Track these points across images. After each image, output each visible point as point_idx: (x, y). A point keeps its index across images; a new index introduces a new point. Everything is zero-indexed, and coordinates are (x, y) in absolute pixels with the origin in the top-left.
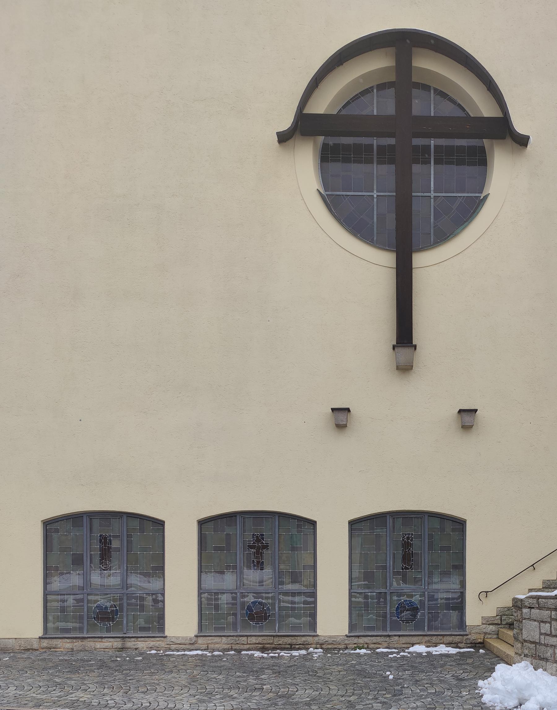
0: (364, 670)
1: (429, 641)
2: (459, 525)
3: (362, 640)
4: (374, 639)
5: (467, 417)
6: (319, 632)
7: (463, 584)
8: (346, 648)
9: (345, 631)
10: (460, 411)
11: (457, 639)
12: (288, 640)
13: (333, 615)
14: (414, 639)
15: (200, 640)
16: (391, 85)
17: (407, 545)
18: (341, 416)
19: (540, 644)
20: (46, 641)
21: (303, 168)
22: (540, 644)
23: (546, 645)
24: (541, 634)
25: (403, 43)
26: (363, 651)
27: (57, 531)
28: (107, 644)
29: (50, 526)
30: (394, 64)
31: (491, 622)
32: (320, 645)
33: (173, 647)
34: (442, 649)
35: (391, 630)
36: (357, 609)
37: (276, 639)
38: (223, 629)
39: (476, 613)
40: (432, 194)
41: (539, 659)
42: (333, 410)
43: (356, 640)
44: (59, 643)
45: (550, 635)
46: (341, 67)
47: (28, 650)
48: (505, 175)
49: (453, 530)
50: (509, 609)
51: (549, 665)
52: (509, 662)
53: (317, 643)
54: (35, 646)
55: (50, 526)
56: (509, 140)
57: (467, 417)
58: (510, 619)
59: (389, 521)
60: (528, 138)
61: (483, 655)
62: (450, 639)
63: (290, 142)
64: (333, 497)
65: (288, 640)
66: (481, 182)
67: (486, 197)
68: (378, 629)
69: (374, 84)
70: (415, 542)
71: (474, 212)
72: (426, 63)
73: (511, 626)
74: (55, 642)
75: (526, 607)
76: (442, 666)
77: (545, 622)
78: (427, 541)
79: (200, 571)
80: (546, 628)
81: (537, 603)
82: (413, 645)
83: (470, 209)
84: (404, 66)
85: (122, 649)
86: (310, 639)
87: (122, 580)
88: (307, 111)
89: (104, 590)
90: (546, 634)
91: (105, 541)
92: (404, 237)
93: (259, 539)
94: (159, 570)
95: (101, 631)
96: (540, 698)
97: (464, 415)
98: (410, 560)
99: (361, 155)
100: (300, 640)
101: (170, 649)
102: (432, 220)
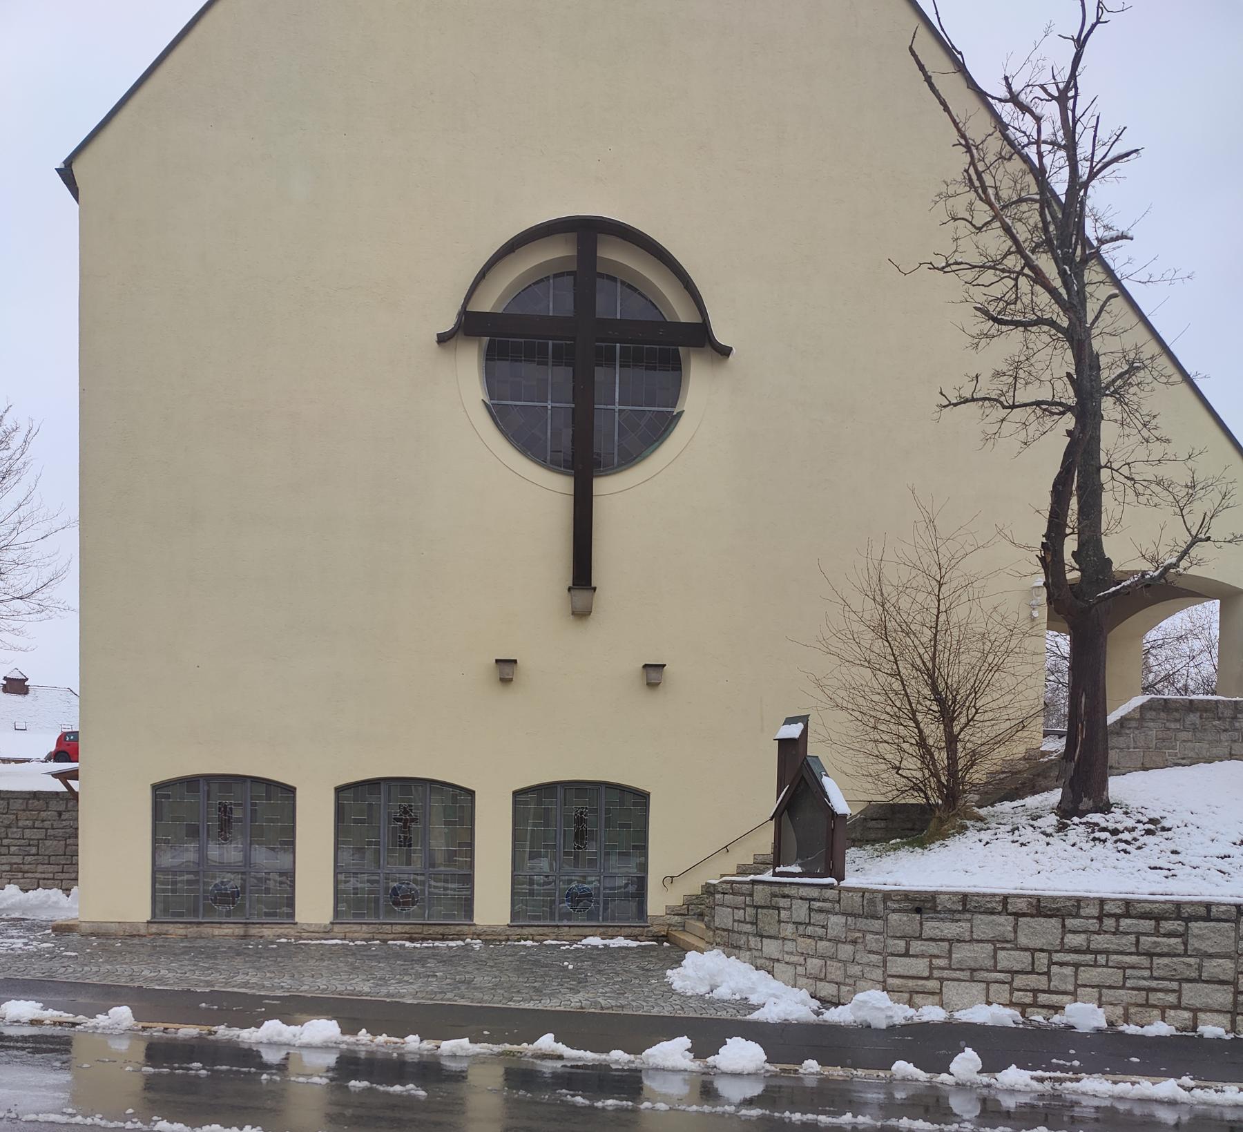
0: (539, 961)
1: (604, 933)
2: (641, 798)
3: (526, 931)
4: (540, 930)
6: (476, 921)
7: (644, 867)
8: (508, 940)
9: (507, 920)
10: (646, 666)
11: (637, 931)
13: (493, 901)
14: (587, 931)
15: (337, 928)
16: (569, 273)
17: (580, 820)
18: (506, 668)
19: (733, 931)
20: (155, 926)
21: (466, 372)
22: (733, 931)
23: (739, 933)
24: (734, 921)
25: (587, 232)
26: (529, 943)
27: (168, 797)
28: (227, 930)
29: (161, 791)
30: (575, 253)
32: (478, 936)
33: (305, 935)
35: (560, 920)
36: (349, 903)
37: (426, 928)
39: (658, 902)
40: (617, 407)
41: (732, 947)
42: (497, 661)
43: (519, 931)
44: (170, 928)
45: (744, 922)
46: (513, 255)
47: (134, 936)
48: (702, 392)
49: (635, 804)
50: (697, 897)
51: (742, 953)
52: (701, 951)
53: (474, 934)
54: (143, 932)
55: (161, 791)
56: (708, 348)
57: (653, 673)
58: (701, 906)
60: (731, 349)
61: (669, 946)
62: (629, 931)
63: (452, 341)
64: (495, 764)
66: (674, 392)
67: (680, 414)
68: (545, 919)
69: (551, 274)
70: (589, 817)
71: (665, 430)
72: (612, 254)
73: (701, 916)
74: (165, 927)
75: (719, 892)
76: (623, 958)
77: (739, 909)
78: (603, 816)
79: (337, 849)
80: (739, 914)
81: (731, 888)
82: (585, 937)
83: (657, 427)
84: (587, 253)
85: (245, 937)
87: (245, 856)
88: (474, 307)
89: (223, 867)
90: (739, 921)
91: (225, 810)
92: (583, 456)
94: (288, 842)
95: (220, 915)
96: (732, 984)
97: (650, 670)
98: (583, 838)
99: (535, 354)
100: (454, 930)
101: (301, 938)
102: (616, 438)
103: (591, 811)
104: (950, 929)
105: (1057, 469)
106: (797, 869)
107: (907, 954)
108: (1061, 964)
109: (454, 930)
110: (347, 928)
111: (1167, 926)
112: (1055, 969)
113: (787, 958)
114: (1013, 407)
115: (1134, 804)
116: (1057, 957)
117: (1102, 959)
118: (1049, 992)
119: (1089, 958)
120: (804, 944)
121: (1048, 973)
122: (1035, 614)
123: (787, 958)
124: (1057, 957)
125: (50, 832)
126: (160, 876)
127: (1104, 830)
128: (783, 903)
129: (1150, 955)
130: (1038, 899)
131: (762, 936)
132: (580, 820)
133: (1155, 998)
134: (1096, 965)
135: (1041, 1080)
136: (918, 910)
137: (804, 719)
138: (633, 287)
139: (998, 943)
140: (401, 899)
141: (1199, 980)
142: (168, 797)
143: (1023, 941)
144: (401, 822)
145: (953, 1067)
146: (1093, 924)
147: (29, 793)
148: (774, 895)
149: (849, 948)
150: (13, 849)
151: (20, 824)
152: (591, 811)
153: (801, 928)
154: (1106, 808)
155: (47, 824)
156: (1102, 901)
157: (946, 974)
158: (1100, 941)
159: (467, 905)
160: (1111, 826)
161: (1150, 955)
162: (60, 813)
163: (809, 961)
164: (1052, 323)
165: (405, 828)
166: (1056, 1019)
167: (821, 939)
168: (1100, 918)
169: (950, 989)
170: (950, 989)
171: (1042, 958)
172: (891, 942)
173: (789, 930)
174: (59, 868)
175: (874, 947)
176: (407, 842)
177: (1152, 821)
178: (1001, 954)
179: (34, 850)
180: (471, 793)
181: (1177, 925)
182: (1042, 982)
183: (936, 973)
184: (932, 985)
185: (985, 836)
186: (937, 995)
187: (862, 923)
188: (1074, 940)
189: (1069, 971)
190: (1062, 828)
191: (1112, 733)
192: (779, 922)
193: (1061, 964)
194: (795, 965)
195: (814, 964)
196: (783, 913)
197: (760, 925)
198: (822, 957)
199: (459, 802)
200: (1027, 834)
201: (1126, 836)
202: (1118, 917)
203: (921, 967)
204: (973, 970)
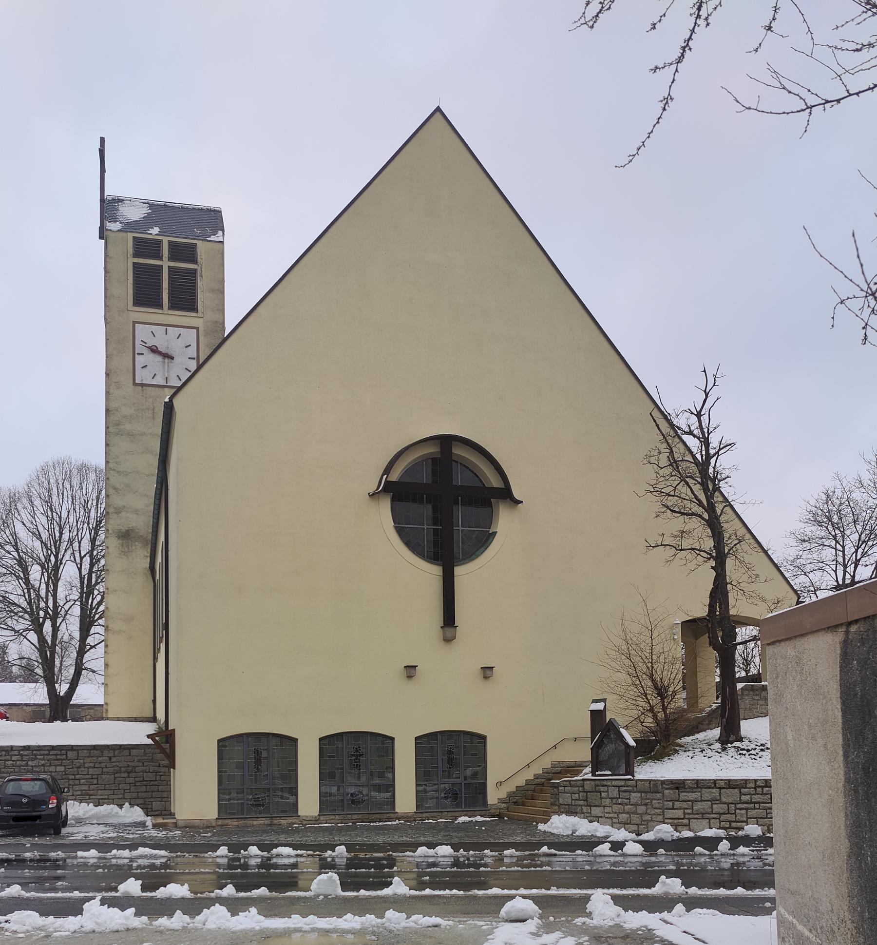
6: (397, 810)
12: (378, 816)
15: (322, 818)
17: (450, 752)
21: (384, 509)
25: (446, 441)
30: (439, 450)
34: (479, 819)
36: (326, 804)
38: (335, 810)
39: (494, 796)
40: (461, 528)
43: (421, 815)
44: (229, 822)
45: (579, 800)
47: (208, 827)
48: (505, 523)
49: (479, 743)
50: (514, 793)
54: (214, 824)
57: (487, 671)
59: (439, 737)
64: (405, 723)
65: (378, 816)
66: (490, 519)
67: (495, 533)
72: (458, 451)
74: (226, 821)
83: (485, 539)
85: (271, 825)
86: (392, 815)
91: (257, 753)
100: (386, 816)
103: (456, 747)
104: (692, 796)
105: (711, 586)
106: (610, 773)
107: (673, 808)
108: (741, 809)
109: (386, 816)
110: (327, 817)
112: (738, 811)
113: (607, 815)
114: (681, 550)
115: (752, 738)
116: (738, 806)
117: (757, 806)
118: (736, 821)
119: (752, 805)
120: (616, 808)
121: (735, 813)
122: (676, 637)
123: (607, 815)
124: (738, 806)
125: (105, 770)
126: (165, 794)
127: (743, 749)
128: (602, 789)
130: (729, 781)
131: (590, 806)
132: (450, 752)
134: (755, 809)
135: (753, 851)
136: (677, 788)
137: (604, 700)
138: (467, 467)
139: (713, 801)
140: (355, 801)
142: (225, 746)
143: (724, 799)
144: (356, 757)
145: (719, 848)
146: (752, 791)
147: (91, 746)
148: (597, 786)
149: (644, 808)
150: (82, 781)
151: (86, 765)
152: (456, 747)
153: (614, 801)
154: (741, 740)
155: (103, 765)
156: (756, 781)
157: (691, 816)
158: (756, 798)
159: (392, 803)
160: (746, 748)
162: (110, 758)
163: (620, 816)
164: (700, 516)
165: (357, 757)
166: (740, 833)
167: (627, 804)
168: (755, 788)
169: (693, 823)
170: (693, 823)
171: (732, 807)
172: (666, 803)
173: (608, 802)
174: (111, 792)
175: (657, 806)
176: (358, 767)
177: (762, 745)
178: (715, 806)
179: (95, 781)
180: (393, 739)
182: (733, 817)
183: (687, 816)
184: (685, 821)
185: (690, 754)
186: (688, 827)
187: (649, 796)
189: (744, 812)
190: (724, 749)
192: (601, 798)
193: (741, 809)
194: (611, 818)
195: (623, 817)
196: (603, 794)
197: (589, 800)
198: (628, 813)
200: (710, 753)
201: (753, 752)
202: (762, 787)
203: (680, 813)
204: (703, 814)
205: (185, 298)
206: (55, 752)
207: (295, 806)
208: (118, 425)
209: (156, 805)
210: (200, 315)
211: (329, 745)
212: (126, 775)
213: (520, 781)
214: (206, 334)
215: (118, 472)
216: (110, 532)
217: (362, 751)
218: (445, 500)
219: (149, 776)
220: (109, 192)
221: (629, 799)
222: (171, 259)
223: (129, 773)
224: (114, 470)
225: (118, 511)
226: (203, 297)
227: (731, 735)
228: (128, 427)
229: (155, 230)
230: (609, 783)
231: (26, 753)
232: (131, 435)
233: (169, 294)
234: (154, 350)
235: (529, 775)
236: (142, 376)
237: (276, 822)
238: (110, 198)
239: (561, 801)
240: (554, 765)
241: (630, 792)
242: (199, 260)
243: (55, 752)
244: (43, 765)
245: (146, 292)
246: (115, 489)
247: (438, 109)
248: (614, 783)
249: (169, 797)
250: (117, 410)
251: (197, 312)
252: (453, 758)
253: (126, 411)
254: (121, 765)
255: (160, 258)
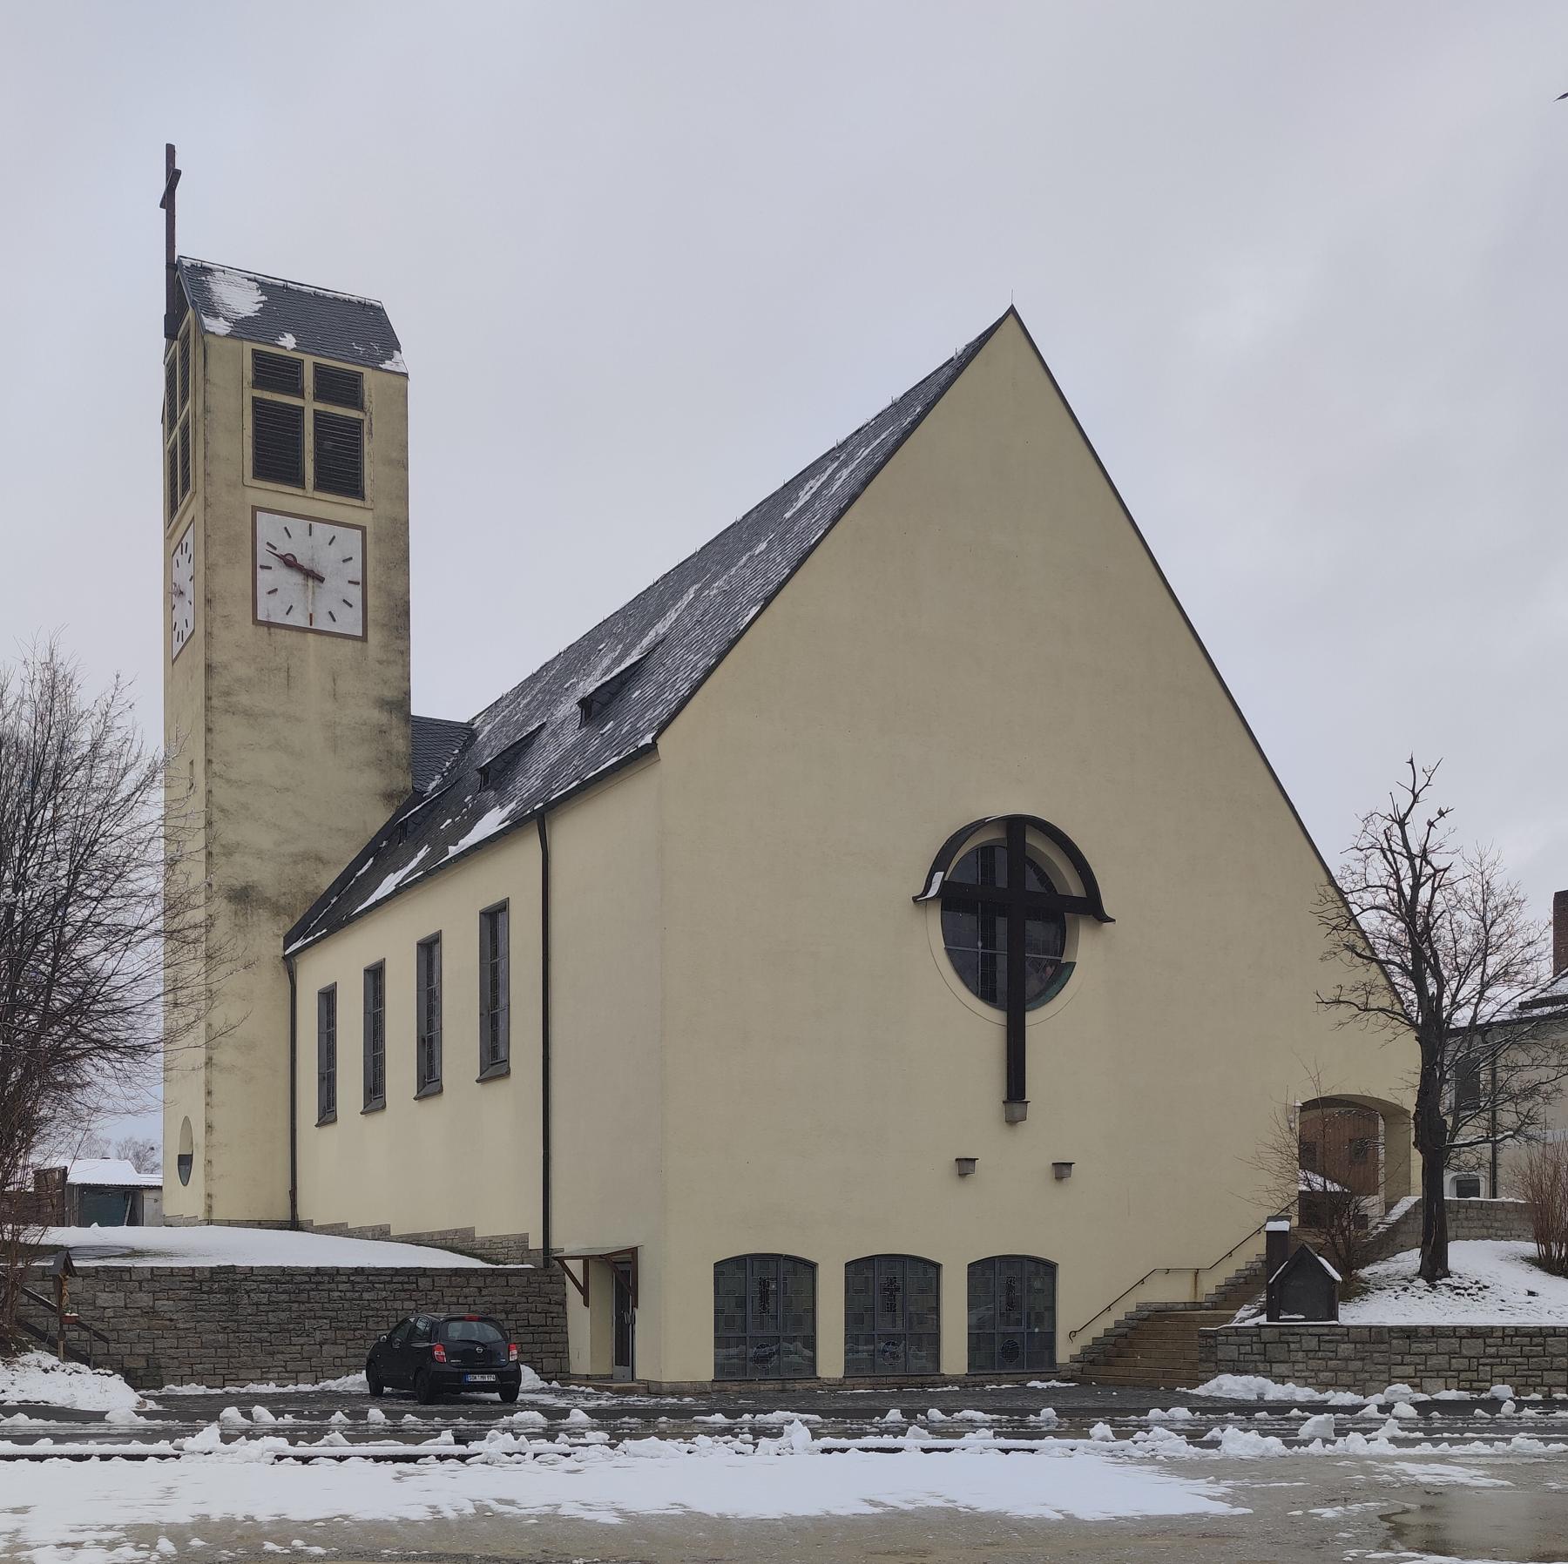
5: (1062, 1170)
6: (944, 1370)
25: (1016, 826)
31: (449, 1243)
39: (1065, 1351)
48: (1088, 950)
64: (955, 1237)
66: (1060, 942)
72: (1034, 841)
83: (1060, 973)
85: (783, 1391)
91: (764, 1284)
93: (892, 1281)
104: (1426, 1347)
111: (1536, 1340)
120: (1313, 1364)
126: (560, 1347)
128: (1291, 1339)
129: (1528, 1357)
131: (1271, 1362)
133: (1530, 1380)
139: (1452, 1354)
141: (1551, 1369)
144: (892, 1290)
149: (1359, 1363)
151: (446, 1300)
153: (1311, 1355)
154: (1448, 1274)
155: (470, 1300)
158: (1504, 1350)
161: (1528, 1357)
163: (1321, 1375)
169: (1427, 1383)
170: (1427, 1383)
176: (892, 1308)
180: (938, 1266)
181: (1540, 1340)
182: (1473, 1376)
187: (1368, 1347)
188: (1492, 1350)
191: (277, 910)
199: (809, 1268)
205: (342, 472)
206: (401, 1279)
207: (813, 1361)
208: (228, 694)
209: (549, 1364)
210: (368, 504)
211: (856, 1269)
212: (503, 1316)
213: (1098, 1330)
214: (379, 540)
215: (228, 781)
216: (215, 888)
217: (899, 1283)
218: (1011, 909)
219: (535, 1319)
220: (186, 249)
221: (1336, 1352)
222: (318, 397)
223: (507, 1313)
224: (221, 777)
225: (229, 851)
226: (372, 471)
227: (1434, 1269)
228: (244, 699)
229: (289, 341)
230: (1302, 1331)
231: (358, 1279)
232: (248, 714)
233: (317, 461)
234: (290, 562)
235: (1108, 1322)
236: (269, 608)
237: (788, 1386)
238: (186, 263)
239: (1220, 1356)
240: (1140, 1308)
241: (1338, 1342)
242: (367, 404)
243: (401, 1279)
244: (384, 1299)
245: (275, 458)
246: (223, 811)
247: (1012, 310)
248: (1311, 1330)
249: (566, 1351)
250: (225, 667)
251: (363, 498)
252: (1016, 1292)
253: (241, 670)
254: (497, 1300)
255: (300, 394)
